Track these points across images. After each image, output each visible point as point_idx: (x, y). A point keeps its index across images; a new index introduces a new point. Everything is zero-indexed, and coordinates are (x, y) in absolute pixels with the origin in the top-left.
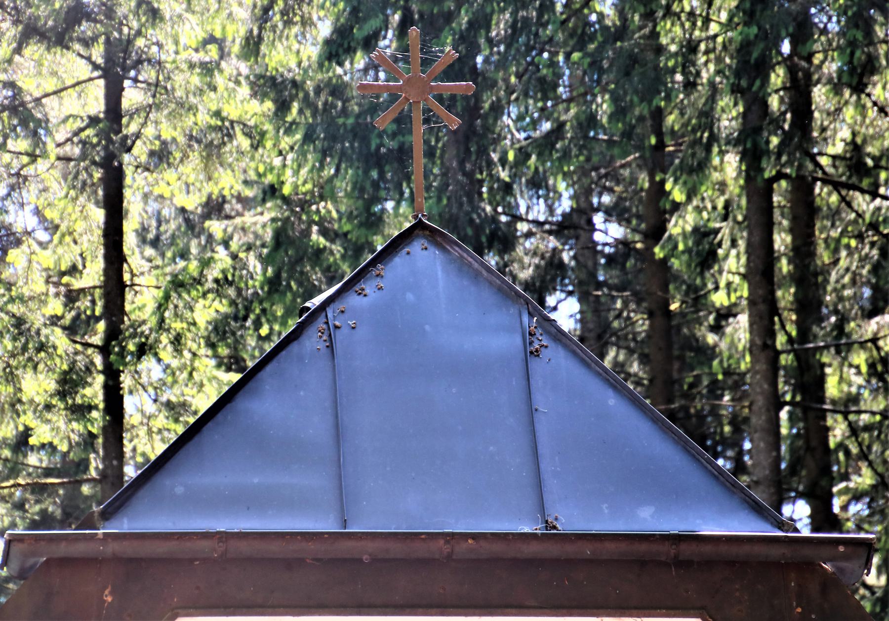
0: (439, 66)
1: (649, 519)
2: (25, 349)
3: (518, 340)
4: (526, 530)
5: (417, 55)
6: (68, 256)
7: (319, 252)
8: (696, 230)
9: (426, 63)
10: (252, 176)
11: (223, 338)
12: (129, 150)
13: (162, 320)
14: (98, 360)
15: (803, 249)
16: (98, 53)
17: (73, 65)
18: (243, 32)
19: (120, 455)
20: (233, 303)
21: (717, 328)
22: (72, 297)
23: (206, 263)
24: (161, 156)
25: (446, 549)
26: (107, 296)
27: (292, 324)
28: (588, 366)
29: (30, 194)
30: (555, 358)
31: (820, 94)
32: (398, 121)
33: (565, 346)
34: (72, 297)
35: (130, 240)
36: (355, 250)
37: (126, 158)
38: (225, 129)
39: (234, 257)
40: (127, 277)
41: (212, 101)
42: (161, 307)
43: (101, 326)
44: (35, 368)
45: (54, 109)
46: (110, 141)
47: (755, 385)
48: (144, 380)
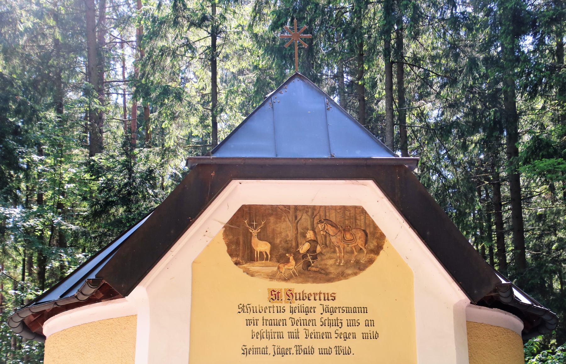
0: (302, 30)
1: (359, 154)
2: (191, 110)
3: (324, 106)
4: (326, 157)
5: (296, 28)
6: (202, 85)
7: (269, 83)
8: (371, 78)
9: (298, 29)
10: (251, 63)
11: (243, 107)
12: (218, 56)
13: (227, 102)
14: (210, 113)
15: (400, 83)
16: (209, 29)
17: (203, 33)
18: (248, 23)
19: (217, 139)
20: (246, 98)
21: (376, 104)
22: (203, 96)
23: (239, 87)
24: (227, 57)
25: (304, 162)
26: (212, 96)
27: (261, 102)
28: (342, 112)
29: (192, 69)
30: (334, 110)
31: (405, 41)
32: (290, 46)
33: (336, 107)
34: (203, 96)
35: (218, 80)
36: (278, 84)
37: (217, 58)
38: (244, 50)
39: (246, 85)
40: (218, 91)
41: (240, 42)
42: (227, 98)
43: (211, 104)
44: (194, 115)
45: (198, 45)
46: (213, 53)
47: (387, 118)
48: (222, 118)
